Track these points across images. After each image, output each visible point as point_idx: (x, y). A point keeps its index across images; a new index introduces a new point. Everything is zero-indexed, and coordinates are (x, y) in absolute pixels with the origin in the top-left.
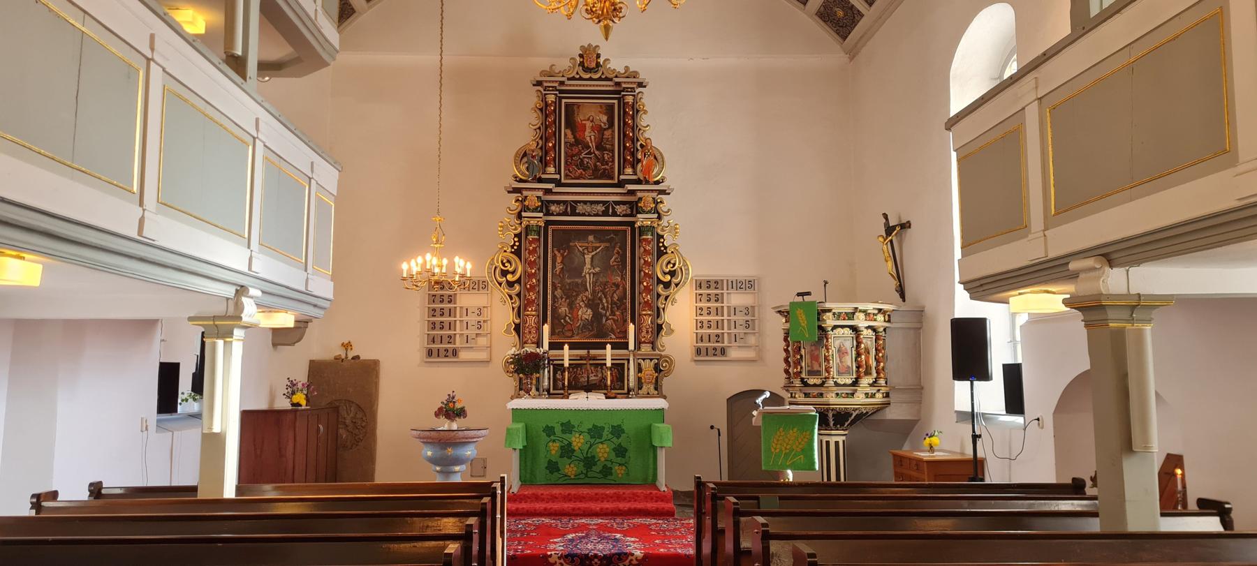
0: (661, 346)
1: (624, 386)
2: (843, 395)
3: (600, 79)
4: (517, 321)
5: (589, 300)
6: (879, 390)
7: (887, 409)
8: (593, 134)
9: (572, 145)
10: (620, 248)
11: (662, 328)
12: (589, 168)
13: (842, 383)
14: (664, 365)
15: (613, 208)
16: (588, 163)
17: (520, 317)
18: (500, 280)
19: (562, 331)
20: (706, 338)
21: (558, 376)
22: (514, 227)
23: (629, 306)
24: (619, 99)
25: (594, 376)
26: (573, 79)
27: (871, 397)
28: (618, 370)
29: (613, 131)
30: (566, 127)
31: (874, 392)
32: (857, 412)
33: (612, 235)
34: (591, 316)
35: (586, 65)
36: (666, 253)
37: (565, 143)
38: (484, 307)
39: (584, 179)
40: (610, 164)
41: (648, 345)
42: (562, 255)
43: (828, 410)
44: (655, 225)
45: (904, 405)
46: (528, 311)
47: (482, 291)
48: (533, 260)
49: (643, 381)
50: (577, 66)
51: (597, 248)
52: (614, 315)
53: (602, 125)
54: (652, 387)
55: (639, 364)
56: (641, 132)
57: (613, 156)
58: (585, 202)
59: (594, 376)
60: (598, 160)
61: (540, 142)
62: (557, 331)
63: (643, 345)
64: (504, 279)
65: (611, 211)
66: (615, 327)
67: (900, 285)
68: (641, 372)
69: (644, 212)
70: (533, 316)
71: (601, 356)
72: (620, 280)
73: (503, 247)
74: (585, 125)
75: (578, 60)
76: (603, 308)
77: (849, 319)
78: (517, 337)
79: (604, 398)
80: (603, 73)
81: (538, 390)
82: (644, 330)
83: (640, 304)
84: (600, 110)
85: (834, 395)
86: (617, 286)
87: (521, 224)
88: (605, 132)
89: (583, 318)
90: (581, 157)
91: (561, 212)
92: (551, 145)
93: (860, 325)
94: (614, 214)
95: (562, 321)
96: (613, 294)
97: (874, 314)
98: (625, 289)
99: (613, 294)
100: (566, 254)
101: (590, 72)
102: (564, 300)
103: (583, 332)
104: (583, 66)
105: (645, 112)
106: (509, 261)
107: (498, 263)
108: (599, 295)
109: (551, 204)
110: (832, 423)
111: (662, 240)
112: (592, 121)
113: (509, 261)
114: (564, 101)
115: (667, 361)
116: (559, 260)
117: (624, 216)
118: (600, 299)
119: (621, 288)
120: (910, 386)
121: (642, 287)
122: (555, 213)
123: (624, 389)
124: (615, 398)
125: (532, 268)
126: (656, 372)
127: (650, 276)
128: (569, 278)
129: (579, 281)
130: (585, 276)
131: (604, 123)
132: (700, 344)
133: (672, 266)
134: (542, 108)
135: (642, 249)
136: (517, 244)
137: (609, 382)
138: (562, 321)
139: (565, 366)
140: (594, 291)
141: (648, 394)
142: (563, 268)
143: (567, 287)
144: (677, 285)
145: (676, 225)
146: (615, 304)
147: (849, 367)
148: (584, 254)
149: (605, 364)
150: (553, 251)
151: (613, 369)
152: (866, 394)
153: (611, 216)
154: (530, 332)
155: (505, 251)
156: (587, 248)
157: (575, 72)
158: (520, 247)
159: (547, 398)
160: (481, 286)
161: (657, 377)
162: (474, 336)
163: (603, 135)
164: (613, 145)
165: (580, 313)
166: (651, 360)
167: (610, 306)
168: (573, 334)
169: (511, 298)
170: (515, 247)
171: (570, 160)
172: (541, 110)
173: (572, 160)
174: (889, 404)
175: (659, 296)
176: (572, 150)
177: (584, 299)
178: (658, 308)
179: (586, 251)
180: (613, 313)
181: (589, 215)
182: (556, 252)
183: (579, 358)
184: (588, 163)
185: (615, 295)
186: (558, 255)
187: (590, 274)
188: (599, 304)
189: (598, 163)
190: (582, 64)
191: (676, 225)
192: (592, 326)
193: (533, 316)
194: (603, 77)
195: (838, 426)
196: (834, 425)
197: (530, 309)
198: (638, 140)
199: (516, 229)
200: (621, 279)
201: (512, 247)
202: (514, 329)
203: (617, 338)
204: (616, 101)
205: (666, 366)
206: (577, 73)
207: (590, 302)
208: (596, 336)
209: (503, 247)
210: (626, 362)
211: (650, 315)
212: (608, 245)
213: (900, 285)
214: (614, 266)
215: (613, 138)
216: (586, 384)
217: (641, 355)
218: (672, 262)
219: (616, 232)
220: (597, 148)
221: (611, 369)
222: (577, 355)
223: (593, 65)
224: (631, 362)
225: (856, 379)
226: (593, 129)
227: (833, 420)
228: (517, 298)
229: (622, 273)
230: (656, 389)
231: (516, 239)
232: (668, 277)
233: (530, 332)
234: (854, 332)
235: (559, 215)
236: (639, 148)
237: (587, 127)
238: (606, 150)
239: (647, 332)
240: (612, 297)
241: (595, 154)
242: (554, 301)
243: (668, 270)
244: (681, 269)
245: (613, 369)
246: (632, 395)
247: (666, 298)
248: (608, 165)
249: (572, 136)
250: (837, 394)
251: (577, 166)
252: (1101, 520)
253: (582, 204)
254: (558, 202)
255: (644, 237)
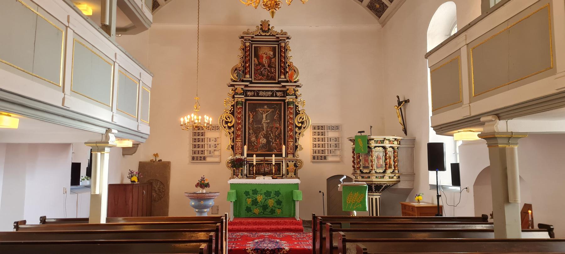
0: (297, 155)
1: (280, 173)
2: (379, 177)
3: (270, 35)
4: (232, 144)
5: (265, 135)
6: (395, 175)
7: (399, 184)
8: (267, 60)
9: (257, 65)
10: (279, 111)
11: (298, 147)
12: (265, 75)
13: (379, 172)
14: (298, 164)
15: (276, 93)
16: (264, 73)
17: (234, 142)
18: (225, 125)
19: (253, 149)
20: (317, 152)
21: (251, 169)
22: (231, 102)
23: (283, 137)
24: (278, 44)
25: (267, 169)
26: (258, 35)
27: (392, 178)
28: (278, 166)
29: (276, 59)
30: (254, 57)
31: (393, 176)
32: (385, 185)
33: (275, 106)
34: (266, 142)
35: (263, 29)
36: (300, 113)
37: (254, 64)
38: (218, 138)
39: (263, 80)
40: (274, 74)
41: (291, 155)
42: (253, 114)
43: (372, 184)
44: (295, 101)
45: (406, 182)
46: (237, 139)
47: (216, 131)
48: (239, 116)
49: (289, 171)
50: (259, 30)
51: (268, 111)
52: (276, 141)
53: (271, 56)
54: (293, 174)
55: (287, 164)
56: (288, 59)
57: (276, 70)
58: (263, 91)
59: (267, 169)
60: (269, 72)
61: (243, 64)
62: (250, 149)
63: (289, 155)
64: (227, 125)
65: (274, 95)
66: (276, 147)
67: (405, 128)
68: (288, 167)
69: (290, 95)
70: (240, 142)
71: (270, 160)
72: (279, 125)
73: (226, 111)
74: (263, 56)
75: (260, 27)
76: (271, 138)
77: (382, 143)
78: (232, 151)
79: (272, 178)
80: (271, 33)
81: (242, 175)
82: (290, 148)
83: (288, 136)
84: (270, 49)
85: (375, 177)
86: (277, 128)
87: (234, 100)
88: (272, 59)
89: (262, 143)
90: (261, 70)
91: (252, 95)
92: (247, 65)
93: (386, 146)
94: (276, 96)
95: (253, 144)
96: (276, 132)
97: (393, 141)
98: (281, 130)
99: (276, 132)
100: (254, 114)
101: (265, 32)
102: (253, 134)
103: (262, 149)
104: (262, 30)
105: (290, 50)
106: (229, 117)
107: (224, 118)
108: (269, 132)
109: (248, 92)
110: (374, 190)
111: (298, 108)
112: (266, 54)
113: (229, 117)
114: (253, 45)
115: (300, 162)
116: (251, 116)
117: (280, 97)
118: (270, 134)
119: (279, 129)
120: (409, 173)
121: (289, 129)
122: (249, 96)
123: (280, 175)
124: (276, 178)
125: (239, 120)
126: (295, 167)
127: (292, 124)
128: (256, 125)
129: (260, 126)
130: (263, 124)
131: (272, 55)
132: (315, 155)
133: (302, 119)
134: (244, 49)
135: (289, 112)
136: (232, 109)
137: (274, 172)
138: (253, 144)
139: (254, 164)
140: (267, 131)
141: (291, 177)
142: (253, 120)
143: (255, 129)
144: (304, 128)
145: (304, 101)
146: (277, 136)
147: (381, 165)
148: (262, 114)
149: (272, 163)
150: (248, 113)
151: (275, 166)
152: (389, 177)
153: (275, 97)
154: (238, 149)
155: (227, 113)
156: (264, 111)
157: (258, 32)
158: (234, 111)
159: (246, 179)
160: (216, 128)
161: (295, 169)
162: (213, 151)
163: (271, 60)
164: (275, 65)
165: (261, 140)
166: (293, 161)
167: (274, 137)
168: (258, 150)
169: (230, 134)
170: (232, 111)
171: (256, 72)
172: (243, 49)
173: (257, 72)
174: (400, 181)
175: (296, 133)
176: (257, 67)
177: (263, 134)
178: (296, 138)
179: (263, 113)
180: (275, 141)
181: (265, 97)
182: (250, 113)
183: (260, 161)
184: (264, 73)
185: (276, 132)
186: (251, 114)
187: (265, 123)
188: (269, 136)
189: (269, 73)
190: (261, 29)
191: (304, 101)
192: (266, 146)
193: (240, 142)
194: (271, 34)
195: (377, 191)
196: (375, 191)
197: (238, 139)
198: (287, 63)
199: (232, 103)
200: (279, 125)
201: (230, 111)
202: (231, 148)
203: (277, 152)
204: (277, 46)
205: (299, 164)
206: (260, 33)
207: (265, 136)
208: (268, 151)
209: (226, 111)
210: (281, 163)
211: (292, 141)
212: (273, 110)
213: (405, 128)
214: (276, 119)
215: (276, 62)
216: (263, 172)
217: (288, 159)
218: (302, 117)
219: (277, 104)
220: (268, 66)
221: (274, 165)
222: (259, 159)
223: (267, 29)
224: (284, 162)
225: (385, 170)
226: (266, 58)
227: (374, 189)
228: (232, 134)
229: (280, 122)
230: (295, 174)
231: (232, 107)
232: (300, 125)
233: (238, 149)
234: (384, 149)
235: (251, 96)
236: (287, 66)
237: (264, 57)
238: (272, 67)
239: (291, 149)
240: (275, 133)
241: (268, 69)
242: (249, 135)
243: (300, 121)
244: (306, 121)
245: (275, 166)
246: (284, 177)
247: (300, 134)
248: (273, 74)
249: (257, 61)
250: (376, 177)
251: (259, 74)
252: (495, 234)
253: (261, 91)
254: (251, 91)
255: (290, 106)
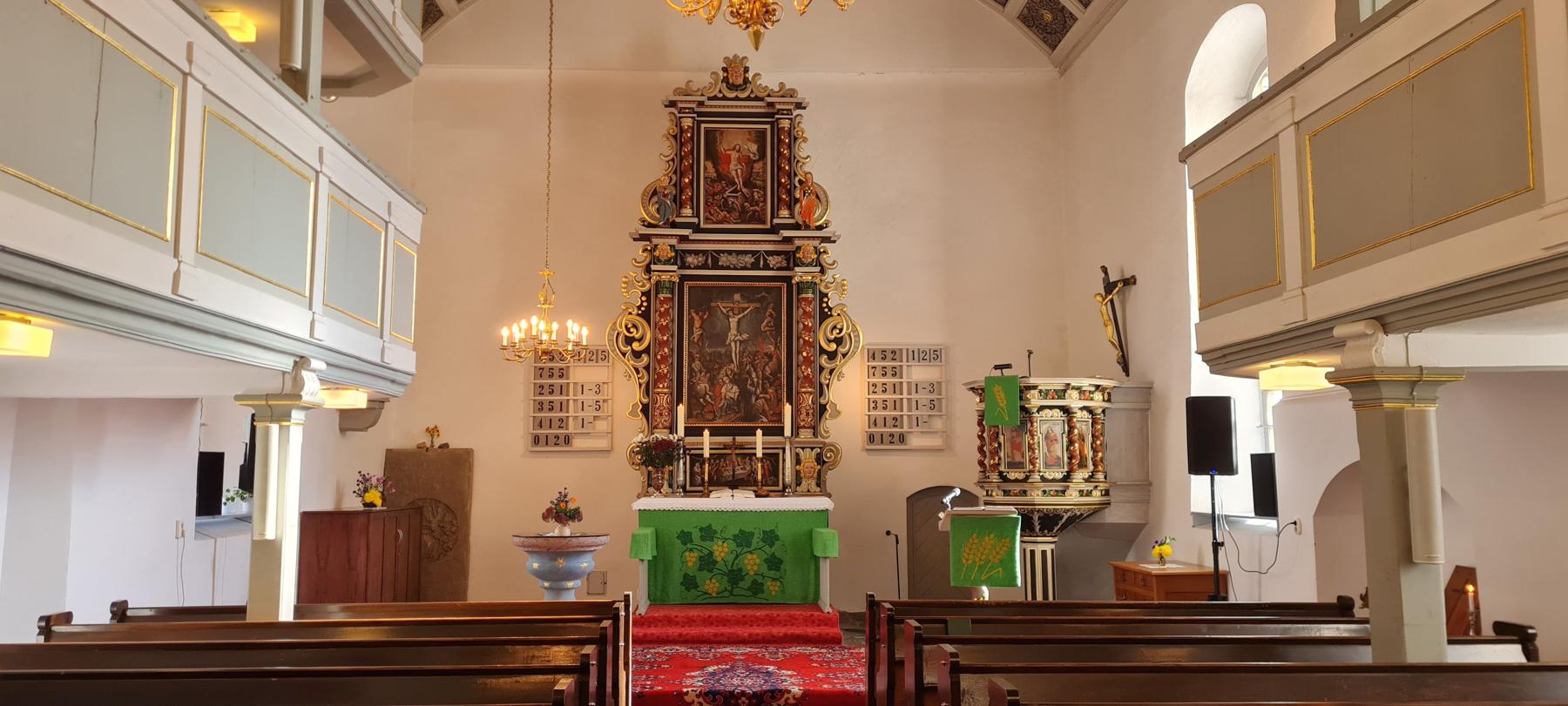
0: (825, 431)
1: (778, 481)
2: (1052, 493)
3: (748, 99)
4: (645, 401)
5: (735, 374)
6: (1096, 487)
7: (1107, 510)
8: (740, 167)
9: (713, 181)
10: (773, 309)
11: (826, 409)
12: (735, 209)
13: (1051, 478)
14: (828, 455)
15: (765, 260)
16: (733, 203)
17: (648, 395)
18: (623, 349)
19: (701, 413)
20: (880, 422)
21: (697, 469)
22: (641, 284)
23: (784, 381)
24: (772, 123)
25: (741, 469)
26: (715, 98)
27: (1087, 495)
28: (771, 462)
29: (765, 164)
30: (706, 159)
31: (1090, 489)
32: (1069, 514)
33: (763, 294)
34: (737, 394)
35: (731, 81)
36: (831, 315)
37: (705, 178)
38: (604, 383)
39: (729, 223)
40: (761, 204)
41: (809, 430)
42: (701, 318)
43: (1032, 511)
44: (818, 281)
45: (1128, 505)
46: (659, 387)
47: (601, 363)
48: (664, 324)
49: (802, 475)
50: (720, 83)
51: (745, 309)
52: (766, 393)
53: (752, 155)
54: (814, 483)
55: (797, 455)
56: (800, 164)
57: (765, 194)
58: (730, 252)
59: (741, 469)
60: (746, 200)
61: (674, 177)
62: (695, 413)
63: (803, 430)
64: (629, 348)
65: (762, 263)
66: (767, 408)
67: (1123, 356)
68: (800, 464)
69: (804, 265)
70: (665, 394)
71: (750, 443)
72: (773, 349)
73: (627, 308)
74: (729, 156)
75: (721, 74)
76: (752, 385)
77: (1059, 398)
78: (644, 420)
79: (754, 496)
80: (752, 91)
81: (671, 486)
82: (804, 412)
83: (798, 379)
84: (749, 137)
85: (1040, 493)
86: (770, 357)
87: (650, 279)
88: (755, 165)
89: (727, 397)
90: (725, 196)
91: (700, 264)
92: (687, 180)
93: (1072, 406)
94: (766, 267)
95: (701, 400)
96: (765, 366)
97: (1090, 392)
98: (779, 361)
99: (765, 366)
100: (705, 316)
101: (737, 90)
102: (703, 374)
103: (727, 414)
104: (728, 83)
105: (805, 140)
106: (634, 326)
107: (621, 328)
108: (748, 368)
109: (687, 255)
110: (1037, 528)
111: (826, 300)
112: (739, 151)
113: (634, 326)
114: (703, 126)
115: (832, 451)
116: (697, 324)
117: (778, 269)
118: (749, 373)
119: (774, 359)
120: (1135, 481)
121: (801, 358)
122: (692, 266)
123: (778, 486)
124: (767, 496)
125: (663, 335)
126: (819, 464)
127: (811, 345)
128: (709, 346)
129: (723, 350)
130: (730, 344)
131: (754, 154)
132: (873, 430)
133: (838, 331)
134: (676, 135)
135: (801, 310)
136: (645, 304)
137: (760, 477)
138: (701, 400)
139: (705, 456)
140: (741, 363)
141: (809, 491)
142: (702, 334)
143: (708, 358)
144: (844, 355)
145: (843, 280)
146: (768, 379)
147: (1059, 458)
148: (728, 317)
149: (755, 454)
150: (690, 314)
151: (764, 460)
152: (1080, 491)
153: (762, 269)
154: (661, 414)
155: (630, 313)
156: (732, 309)
157: (717, 90)
158: (648, 308)
159: (682, 497)
160: (600, 357)
161: (819, 470)
162: (591, 419)
163: (752, 168)
164: (765, 181)
165: (723, 390)
166: (812, 449)
167: (761, 382)
168: (715, 416)
169: (637, 371)
170: (643, 309)
171: (711, 200)
172: (675, 137)
173: (714, 199)
174: (1109, 504)
175: (822, 369)
176: (713, 187)
177: (729, 373)
178: (821, 384)
179: (731, 314)
180: (764, 391)
181: (735, 269)
182: (694, 315)
183: (722, 447)
184: (733, 203)
185: (767, 368)
186: (697, 318)
187: (736, 342)
188: (747, 379)
189: (746, 204)
190: (726, 80)
191: (843, 280)
192: (739, 407)
193: (665, 394)
194: (752, 96)
195: (1046, 531)
196: (1040, 530)
197: (661, 386)
198: (795, 175)
199: (643, 286)
200: (775, 348)
201: (639, 308)
202: (641, 411)
203: (770, 422)
204: (768, 127)
205: (831, 457)
206: (720, 91)
207: (736, 377)
208: (744, 420)
209: (627, 308)
210: (781, 452)
211: (810, 393)
212: (758, 305)
213: (1123, 356)
214: (766, 331)
215: (765, 172)
216: (731, 479)
217: (800, 442)
218: (839, 326)
219: (768, 290)
220: (745, 185)
221: (762, 460)
222: (720, 443)
223: (740, 81)
224: (788, 451)
225: (1068, 472)
226: (739, 160)
227: (1039, 524)
228: (645, 372)
229: (776, 340)
230: (818, 485)
231: (644, 299)
232: (834, 346)
233: (661, 414)
234: (1066, 415)
235: (697, 268)
236: (797, 184)
237: (732, 159)
238: (756, 187)
239: (808, 414)
240: (763, 370)
241: (743, 193)
242: (691, 376)
243: (833, 337)
244: (850, 335)
245: (764, 460)
246: (789, 492)
247: (831, 372)
248: (758, 205)
249: (714, 170)
250: (1044, 492)
251: (719, 207)
252: (1373, 649)
253: (726, 254)
254: (696, 253)
255: (804, 295)
